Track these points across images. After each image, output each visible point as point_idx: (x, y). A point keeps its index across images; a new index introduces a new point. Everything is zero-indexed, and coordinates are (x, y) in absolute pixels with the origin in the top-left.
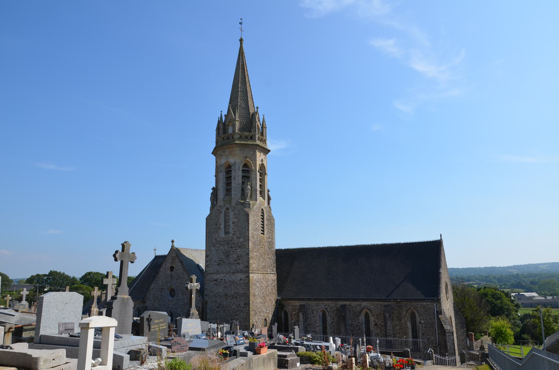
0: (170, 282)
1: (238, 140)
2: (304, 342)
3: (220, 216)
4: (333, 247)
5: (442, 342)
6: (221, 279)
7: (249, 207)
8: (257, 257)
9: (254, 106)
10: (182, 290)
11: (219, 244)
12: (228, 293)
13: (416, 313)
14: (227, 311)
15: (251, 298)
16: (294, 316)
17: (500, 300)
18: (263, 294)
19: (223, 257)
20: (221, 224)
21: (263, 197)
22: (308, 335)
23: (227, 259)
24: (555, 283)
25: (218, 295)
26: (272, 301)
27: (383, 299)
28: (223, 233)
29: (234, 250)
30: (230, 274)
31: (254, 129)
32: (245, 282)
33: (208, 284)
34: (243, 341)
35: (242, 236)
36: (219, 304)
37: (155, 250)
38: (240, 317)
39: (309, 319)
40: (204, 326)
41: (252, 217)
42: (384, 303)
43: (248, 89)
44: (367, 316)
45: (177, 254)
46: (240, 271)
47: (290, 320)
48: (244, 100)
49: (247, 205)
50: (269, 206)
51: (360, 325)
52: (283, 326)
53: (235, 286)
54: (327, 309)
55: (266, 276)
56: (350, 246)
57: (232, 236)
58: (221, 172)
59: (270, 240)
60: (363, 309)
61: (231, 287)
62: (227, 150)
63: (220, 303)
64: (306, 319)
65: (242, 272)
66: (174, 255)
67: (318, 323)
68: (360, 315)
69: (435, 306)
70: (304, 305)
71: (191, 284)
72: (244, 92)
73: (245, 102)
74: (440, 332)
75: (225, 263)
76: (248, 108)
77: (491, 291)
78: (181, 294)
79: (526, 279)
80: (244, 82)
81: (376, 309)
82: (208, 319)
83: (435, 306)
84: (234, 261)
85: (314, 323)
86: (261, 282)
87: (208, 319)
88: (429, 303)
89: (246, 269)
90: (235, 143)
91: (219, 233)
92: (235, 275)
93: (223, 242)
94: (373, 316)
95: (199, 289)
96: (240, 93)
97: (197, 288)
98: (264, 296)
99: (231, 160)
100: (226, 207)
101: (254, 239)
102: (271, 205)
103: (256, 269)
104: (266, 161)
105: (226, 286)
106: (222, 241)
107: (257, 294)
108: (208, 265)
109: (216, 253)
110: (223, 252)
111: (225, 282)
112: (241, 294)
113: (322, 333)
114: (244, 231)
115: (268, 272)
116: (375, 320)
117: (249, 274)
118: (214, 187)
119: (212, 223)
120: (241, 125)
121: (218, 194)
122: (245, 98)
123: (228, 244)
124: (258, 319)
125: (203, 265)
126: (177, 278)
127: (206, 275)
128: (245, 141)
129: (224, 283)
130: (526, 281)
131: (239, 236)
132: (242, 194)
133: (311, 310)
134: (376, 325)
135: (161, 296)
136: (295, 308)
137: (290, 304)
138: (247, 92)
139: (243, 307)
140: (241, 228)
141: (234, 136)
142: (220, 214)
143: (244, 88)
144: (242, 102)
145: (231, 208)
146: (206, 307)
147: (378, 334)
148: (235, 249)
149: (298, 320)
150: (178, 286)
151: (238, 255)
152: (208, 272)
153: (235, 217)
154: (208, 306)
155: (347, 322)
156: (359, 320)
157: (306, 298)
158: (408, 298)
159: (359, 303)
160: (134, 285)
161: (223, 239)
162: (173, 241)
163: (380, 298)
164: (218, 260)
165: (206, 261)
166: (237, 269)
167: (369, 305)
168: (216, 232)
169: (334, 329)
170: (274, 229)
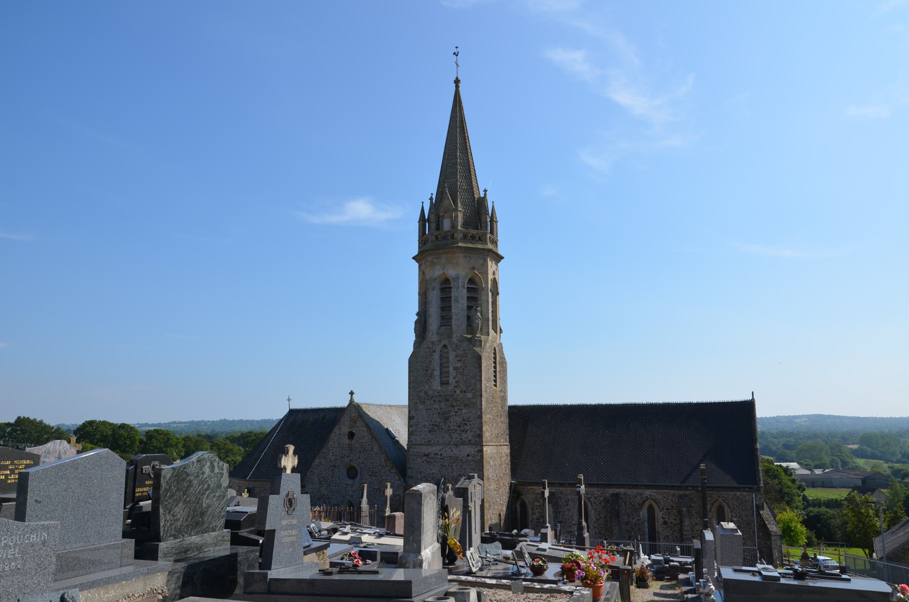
0: (348, 457)
3: (433, 357)
4: (588, 405)
5: (764, 549)
6: (436, 454)
7: (480, 346)
10: (370, 468)
11: (431, 399)
13: (725, 508)
16: (537, 508)
17: (777, 480)
19: (439, 420)
20: (434, 370)
23: (445, 423)
24: (822, 449)
27: (676, 486)
30: (450, 446)
33: (413, 461)
35: (470, 389)
37: (289, 400)
42: (677, 492)
44: (651, 510)
46: (467, 442)
48: (465, 178)
51: (640, 523)
54: (591, 500)
56: (614, 405)
57: (453, 389)
60: (647, 500)
61: (452, 466)
66: (353, 415)
67: (576, 520)
68: (641, 508)
69: (754, 497)
73: (468, 181)
74: (761, 534)
75: (442, 429)
77: (764, 466)
79: (775, 440)
81: (665, 500)
83: (754, 497)
84: (458, 426)
88: (744, 493)
89: (478, 439)
90: (458, 247)
91: (431, 383)
93: (439, 397)
94: (661, 511)
96: (459, 167)
99: (451, 272)
105: (444, 464)
106: (437, 395)
108: (412, 431)
111: (442, 459)
115: (502, 444)
116: (664, 516)
117: (482, 447)
123: (448, 401)
124: (493, 514)
128: (471, 243)
129: (441, 460)
130: (776, 443)
131: (465, 389)
134: (665, 523)
135: (332, 477)
137: (531, 491)
140: (469, 377)
141: (455, 235)
145: (451, 347)
147: (668, 536)
148: (459, 409)
150: (363, 463)
151: (463, 418)
153: (458, 361)
156: (640, 516)
158: (714, 485)
159: (640, 491)
161: (438, 392)
162: (352, 393)
163: (672, 484)
164: (430, 425)
166: (461, 439)
167: (655, 494)
168: (427, 381)
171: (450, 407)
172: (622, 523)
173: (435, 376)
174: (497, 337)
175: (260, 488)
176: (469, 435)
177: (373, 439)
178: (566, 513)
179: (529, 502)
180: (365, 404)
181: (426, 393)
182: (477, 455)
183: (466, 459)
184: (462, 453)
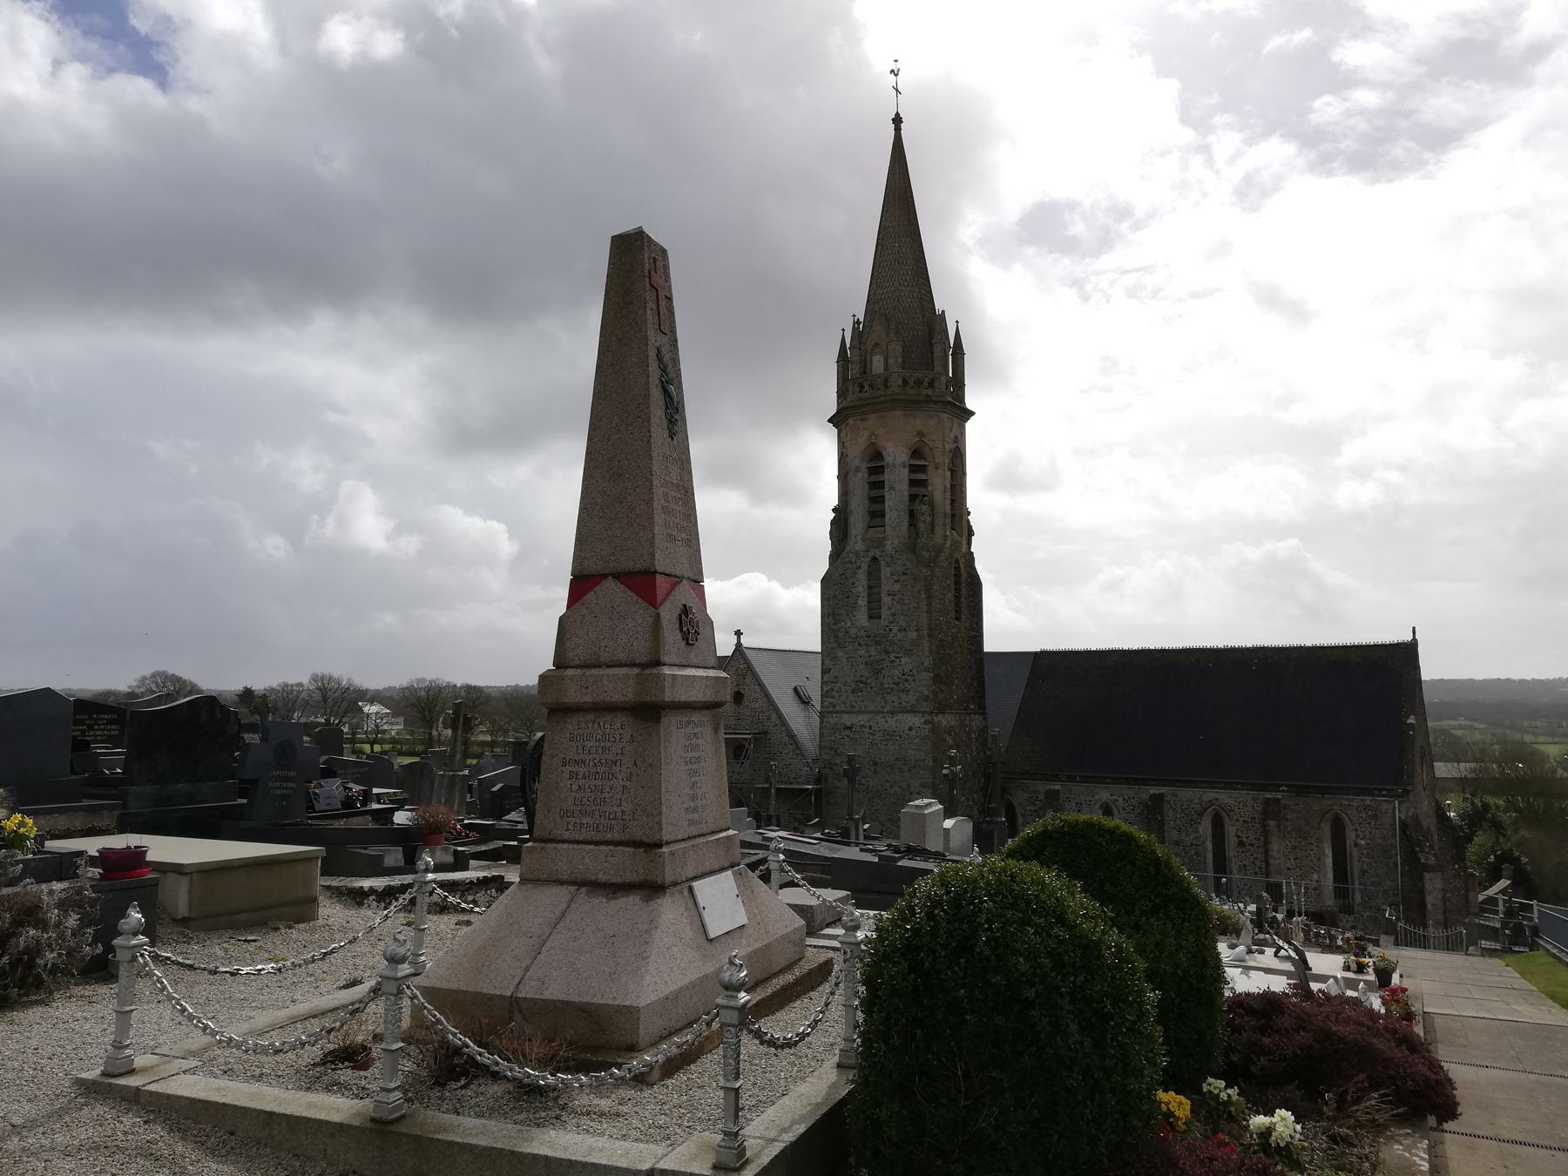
6: (862, 726)
23: (876, 679)
108: (827, 691)
111: (871, 733)
123: (878, 643)
131: (904, 625)
153: (895, 581)
155: (1166, 834)
181: (847, 632)
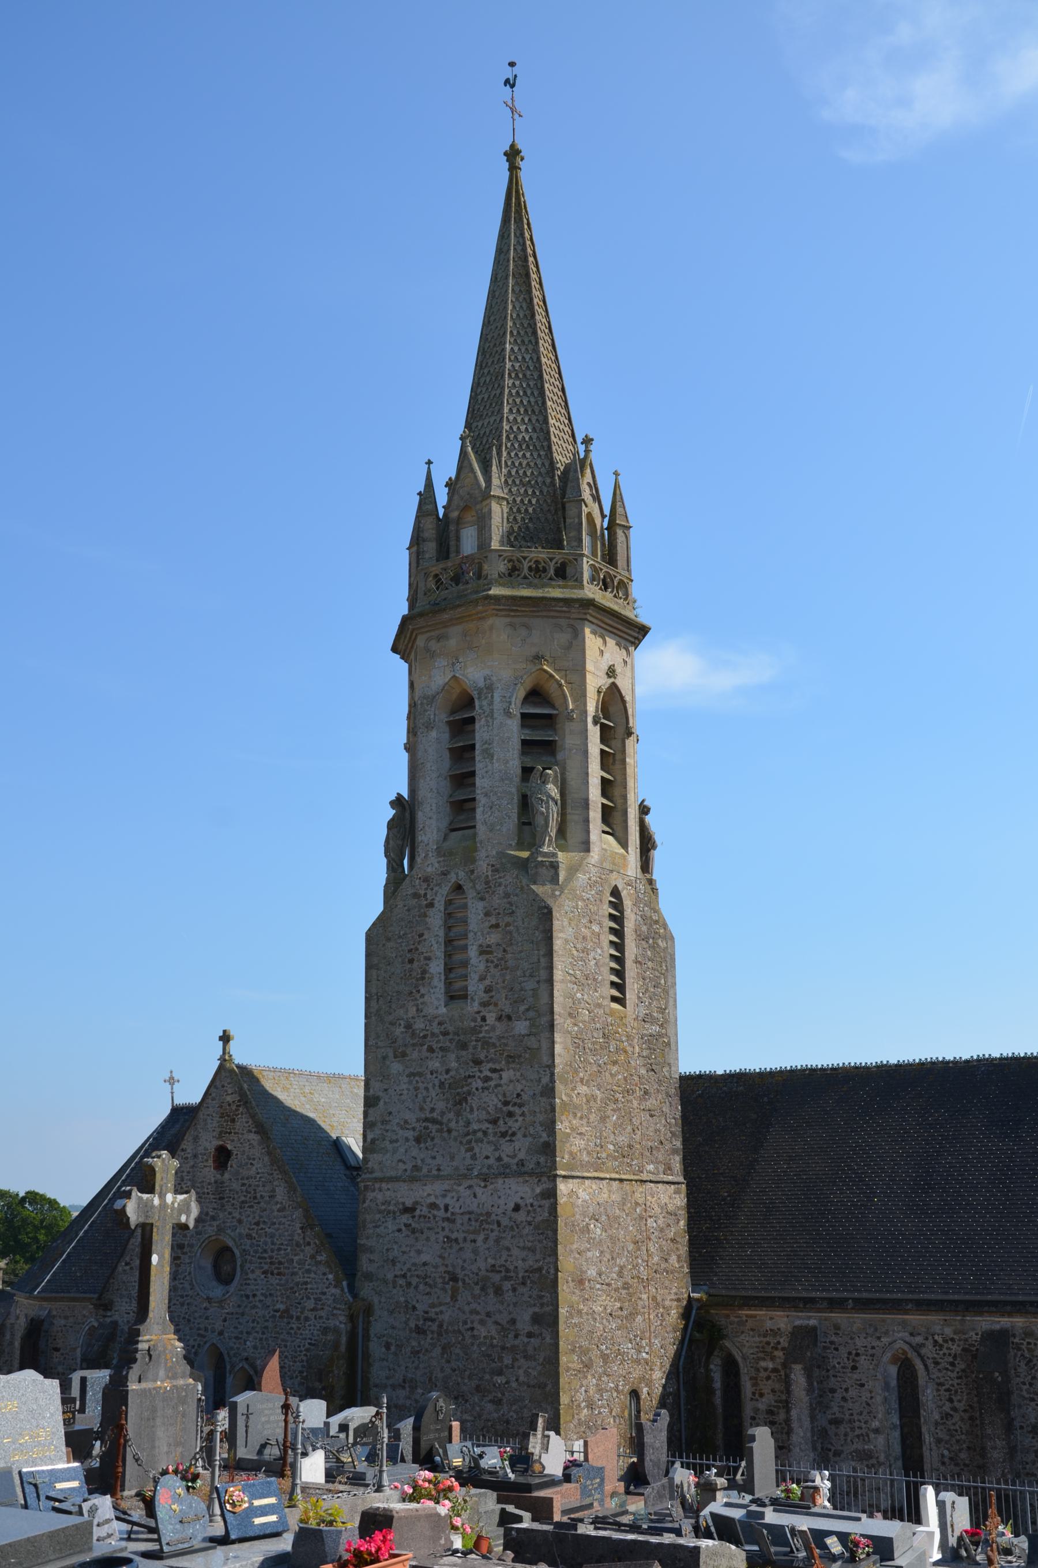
1: (503, 585)
2: (762, 1515)
3: (427, 919)
4: (948, 1062)
6: (433, 1206)
7: (555, 880)
8: (592, 1103)
9: (573, 436)
10: (265, 1251)
11: (422, 1045)
12: (463, 1268)
14: (457, 1351)
15: (566, 1290)
16: (768, 1378)
18: (620, 1274)
19: (441, 1105)
21: (619, 834)
22: (817, 1473)
23: (458, 1114)
25: (418, 1276)
26: (668, 1309)
28: (438, 999)
29: (489, 1074)
31: (573, 534)
32: (539, 1219)
33: (376, 1227)
34: (273, 1518)
35: (522, 1008)
36: (425, 1320)
37: (172, 1081)
38: (517, 1380)
39: (838, 1395)
40: (272, 1418)
41: (566, 923)
43: (544, 360)
45: (242, 1094)
47: (749, 1395)
48: (526, 411)
49: (543, 871)
50: (648, 876)
52: (720, 1426)
53: (493, 1236)
54: (923, 1351)
55: (638, 1195)
57: (478, 1012)
58: (429, 726)
59: (655, 1029)
61: (474, 1241)
62: (455, 631)
63: (427, 1313)
64: (821, 1396)
65: (525, 1173)
66: (229, 1099)
67: (880, 1416)
70: (814, 1329)
71: (145, 1196)
72: (528, 373)
75: (449, 1131)
76: (545, 444)
78: (258, 1272)
80: (529, 330)
82: (376, 1386)
84: (490, 1123)
85: (861, 1413)
86: (613, 1221)
87: (376, 1386)
89: (542, 1160)
90: (488, 597)
92: (492, 1186)
95: (191, 1225)
96: (508, 382)
97: (183, 1219)
98: (626, 1286)
99: (473, 674)
100: (453, 881)
101: (576, 1025)
102: (658, 872)
103: (585, 1157)
104: (629, 674)
105: (453, 1236)
106: (436, 1031)
107: (592, 1272)
108: (373, 1141)
109: (408, 1090)
110: (442, 1084)
111: (448, 1219)
112: (520, 1275)
113: (900, 1463)
114: (530, 985)
115: (644, 1176)
117: (555, 1181)
118: (399, 797)
119: (394, 955)
120: (515, 519)
121: (419, 825)
122: (532, 400)
123: (463, 1046)
124: (600, 1391)
125: (355, 1144)
126: (243, 1198)
127: (366, 1187)
128: (530, 585)
129: (445, 1224)
131: (508, 1010)
132: (524, 824)
133: (843, 1352)
136: (773, 1341)
138: (541, 376)
139: (530, 1335)
141: (486, 567)
142: (425, 916)
143: (527, 357)
144: (519, 419)
145: (474, 887)
146: (366, 1331)
149: (784, 1397)
150: (249, 1236)
151: (504, 1095)
152: (374, 1175)
153: (492, 926)
154: (377, 1328)
155: (1015, 1413)
157: (821, 1298)
160: (81, 1234)
162: (225, 1038)
165: (368, 1126)
166: (499, 1159)
169: (956, 1447)
170: (670, 980)
171: (471, 1064)
172: (1021, 1427)
173: (432, 978)
174: (624, 858)
175: (66, 1318)
176: (520, 1148)
177: (275, 1167)
178: (853, 1393)
179: (744, 1358)
180: (275, 1070)
181: (408, 1026)
182: (540, 1206)
183: (510, 1218)
184: (501, 1202)
